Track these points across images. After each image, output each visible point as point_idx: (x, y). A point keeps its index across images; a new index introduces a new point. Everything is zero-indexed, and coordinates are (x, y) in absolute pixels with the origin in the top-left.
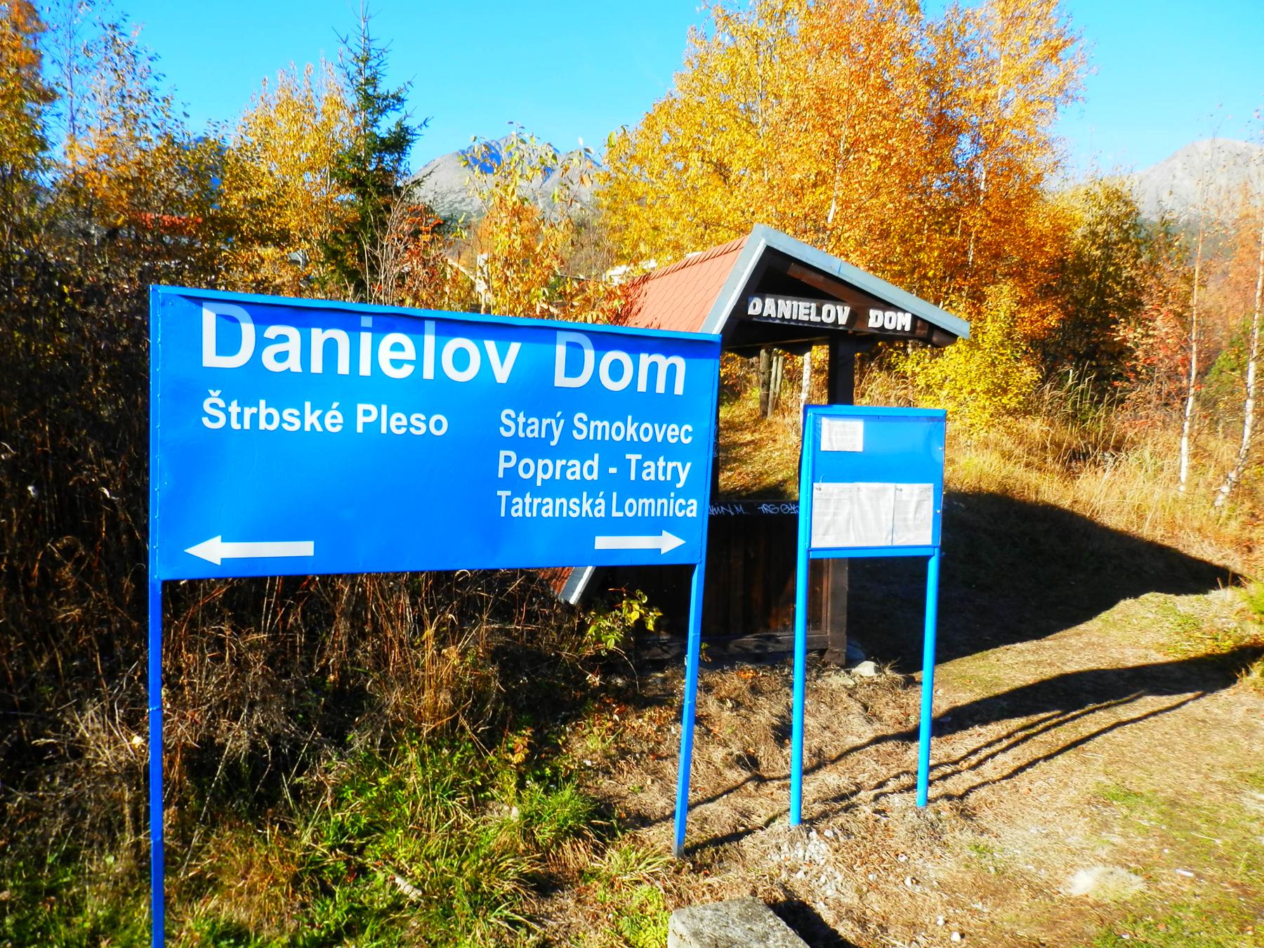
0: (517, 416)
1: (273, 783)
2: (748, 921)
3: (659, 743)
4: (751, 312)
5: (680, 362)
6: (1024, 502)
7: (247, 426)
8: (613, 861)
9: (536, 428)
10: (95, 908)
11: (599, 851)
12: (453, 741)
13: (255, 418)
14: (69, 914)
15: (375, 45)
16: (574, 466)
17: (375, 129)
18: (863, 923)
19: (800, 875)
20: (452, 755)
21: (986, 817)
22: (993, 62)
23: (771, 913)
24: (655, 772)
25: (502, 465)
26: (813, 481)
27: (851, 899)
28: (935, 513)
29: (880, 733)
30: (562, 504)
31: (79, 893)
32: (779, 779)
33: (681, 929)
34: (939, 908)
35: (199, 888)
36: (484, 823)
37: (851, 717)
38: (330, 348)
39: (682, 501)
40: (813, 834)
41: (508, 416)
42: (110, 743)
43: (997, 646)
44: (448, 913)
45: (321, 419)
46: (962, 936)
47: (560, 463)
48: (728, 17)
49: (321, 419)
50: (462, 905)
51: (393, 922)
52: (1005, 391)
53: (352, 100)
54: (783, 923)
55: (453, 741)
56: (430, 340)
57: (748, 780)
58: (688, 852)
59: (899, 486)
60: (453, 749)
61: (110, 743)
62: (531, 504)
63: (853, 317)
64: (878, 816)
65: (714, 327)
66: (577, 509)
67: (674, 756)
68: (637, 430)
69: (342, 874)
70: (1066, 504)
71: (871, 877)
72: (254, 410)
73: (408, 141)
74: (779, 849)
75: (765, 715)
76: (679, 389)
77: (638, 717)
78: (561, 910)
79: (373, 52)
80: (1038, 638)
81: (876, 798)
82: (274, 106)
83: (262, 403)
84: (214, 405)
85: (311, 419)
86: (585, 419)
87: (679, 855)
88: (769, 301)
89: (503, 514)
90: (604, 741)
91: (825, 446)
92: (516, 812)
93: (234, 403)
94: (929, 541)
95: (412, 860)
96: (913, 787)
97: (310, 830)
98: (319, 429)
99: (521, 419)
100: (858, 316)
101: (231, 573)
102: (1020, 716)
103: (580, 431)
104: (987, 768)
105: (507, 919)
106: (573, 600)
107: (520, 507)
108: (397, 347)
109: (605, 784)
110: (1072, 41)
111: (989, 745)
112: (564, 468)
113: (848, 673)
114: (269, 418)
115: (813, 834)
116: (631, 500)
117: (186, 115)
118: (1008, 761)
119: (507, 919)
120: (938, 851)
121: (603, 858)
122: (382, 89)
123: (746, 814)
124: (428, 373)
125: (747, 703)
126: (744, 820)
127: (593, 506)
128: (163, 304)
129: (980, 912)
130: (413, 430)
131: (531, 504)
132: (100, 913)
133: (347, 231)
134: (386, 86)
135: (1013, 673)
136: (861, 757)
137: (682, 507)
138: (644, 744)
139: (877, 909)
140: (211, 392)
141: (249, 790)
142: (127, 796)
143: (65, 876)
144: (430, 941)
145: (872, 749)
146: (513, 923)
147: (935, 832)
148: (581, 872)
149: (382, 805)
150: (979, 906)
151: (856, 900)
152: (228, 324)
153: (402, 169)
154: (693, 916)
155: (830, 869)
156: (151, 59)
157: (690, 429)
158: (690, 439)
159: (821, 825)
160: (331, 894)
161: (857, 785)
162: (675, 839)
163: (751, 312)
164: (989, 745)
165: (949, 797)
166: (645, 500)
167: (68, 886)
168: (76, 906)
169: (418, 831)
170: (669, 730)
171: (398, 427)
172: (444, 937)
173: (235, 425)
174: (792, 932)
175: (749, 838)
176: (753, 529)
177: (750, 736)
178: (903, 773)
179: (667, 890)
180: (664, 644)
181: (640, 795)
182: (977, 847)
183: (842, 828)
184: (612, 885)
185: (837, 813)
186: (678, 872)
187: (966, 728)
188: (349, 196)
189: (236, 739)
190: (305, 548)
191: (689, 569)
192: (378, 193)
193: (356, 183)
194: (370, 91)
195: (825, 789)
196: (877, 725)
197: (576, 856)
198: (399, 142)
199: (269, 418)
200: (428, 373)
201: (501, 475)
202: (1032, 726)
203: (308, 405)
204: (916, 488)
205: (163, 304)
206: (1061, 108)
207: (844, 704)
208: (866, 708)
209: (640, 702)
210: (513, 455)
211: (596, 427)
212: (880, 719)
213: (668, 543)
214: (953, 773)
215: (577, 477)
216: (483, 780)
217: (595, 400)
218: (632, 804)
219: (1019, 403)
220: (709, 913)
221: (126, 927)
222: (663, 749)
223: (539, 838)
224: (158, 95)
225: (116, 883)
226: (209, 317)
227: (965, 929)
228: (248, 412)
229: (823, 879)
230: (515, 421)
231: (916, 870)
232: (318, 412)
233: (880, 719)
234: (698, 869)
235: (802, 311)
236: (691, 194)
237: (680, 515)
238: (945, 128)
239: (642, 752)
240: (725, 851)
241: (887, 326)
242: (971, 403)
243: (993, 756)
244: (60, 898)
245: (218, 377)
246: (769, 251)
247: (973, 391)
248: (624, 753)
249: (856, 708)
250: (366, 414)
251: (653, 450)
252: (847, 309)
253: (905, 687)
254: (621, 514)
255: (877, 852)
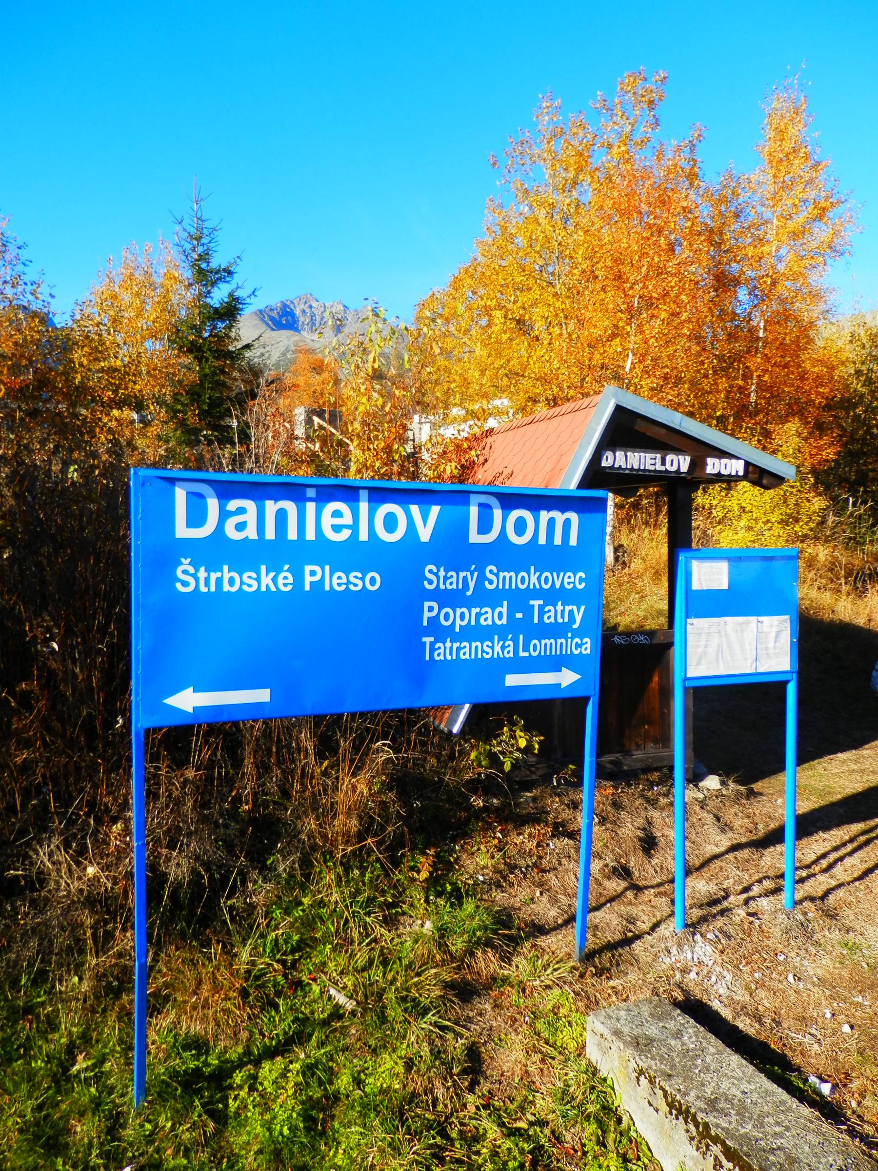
0: (438, 570)
1: (212, 905)
2: (660, 1019)
3: (540, 858)
4: (604, 464)
5: (573, 517)
6: (822, 620)
7: (213, 589)
8: (521, 966)
9: (454, 580)
10: (70, 1024)
11: (506, 959)
12: (361, 862)
13: (219, 581)
14: (46, 1032)
15: (207, 224)
16: (486, 613)
17: (208, 300)
18: (759, 1019)
19: (693, 975)
20: (363, 875)
21: (848, 916)
22: (767, 222)
23: (679, 1011)
24: (541, 885)
25: (426, 615)
26: (687, 617)
27: (742, 996)
28: (792, 642)
29: (735, 842)
30: (476, 647)
31: (53, 1011)
32: (652, 887)
33: (600, 1028)
34: (824, 1002)
35: (154, 1006)
36: (399, 936)
37: (706, 827)
38: (281, 516)
39: (577, 640)
40: (698, 937)
41: (431, 571)
42: (68, 874)
43: (821, 757)
44: (383, 1019)
45: (274, 580)
46: (852, 1027)
47: (474, 611)
48: (526, 191)
49: (274, 580)
50: (395, 1013)
51: (335, 1030)
52: (797, 520)
53: (188, 274)
54: (692, 1021)
55: (361, 862)
56: (364, 506)
57: (626, 889)
58: (588, 957)
59: (760, 618)
60: (363, 870)
61: (68, 874)
62: (451, 648)
63: (693, 465)
64: (751, 919)
65: (570, 482)
66: (490, 650)
67: (555, 869)
68: (539, 579)
69: (283, 987)
70: (861, 621)
71: (756, 975)
72: (219, 574)
73: (238, 309)
74: (669, 952)
75: (630, 828)
76: (573, 541)
77: (519, 834)
78: (480, 1014)
79: (205, 231)
80: (856, 747)
81: (746, 902)
82: (117, 283)
83: (226, 568)
84: (185, 572)
85: (266, 580)
86: (495, 571)
87: (581, 960)
88: (620, 454)
89: (427, 658)
90: (493, 857)
91: (695, 586)
92: (428, 925)
93: (202, 569)
94: (787, 667)
95: (342, 973)
96: (777, 890)
97: (248, 948)
98: (273, 589)
99: (442, 573)
100: (697, 464)
101: (203, 719)
102: (858, 821)
103: (491, 582)
104: (838, 869)
105: (435, 1024)
106: (456, 729)
107: (442, 651)
108: (337, 514)
109: (499, 896)
110: (840, 202)
111: (836, 849)
112: (478, 615)
113: (696, 786)
114: (231, 582)
115: (698, 937)
116: (535, 641)
117: (52, 296)
118: (856, 863)
119: (435, 1024)
120: (812, 949)
121: (510, 965)
122: (214, 264)
123: (631, 920)
124: (363, 536)
125: (612, 818)
126: (631, 927)
127: (503, 648)
128: (143, 484)
129: (861, 1005)
130: (351, 587)
131: (451, 648)
132: (75, 1030)
133: (187, 393)
134: (217, 261)
135: (842, 782)
136: (723, 864)
137: (578, 646)
138: (528, 859)
139: (767, 1005)
140: (183, 560)
141: (192, 915)
142: (88, 922)
143: (39, 996)
144: (370, 1047)
145: (730, 856)
146: (443, 1028)
147: (805, 930)
148: (494, 979)
149: (309, 923)
150: (860, 999)
151: (747, 997)
152: (196, 501)
153: (233, 335)
154: (610, 1017)
155: (718, 969)
156: (19, 248)
157: (584, 576)
158: (583, 584)
159: (704, 928)
160: (276, 1007)
161: (724, 890)
162: (577, 942)
163: (604, 464)
164: (836, 849)
165: (812, 899)
166: (547, 641)
167: (43, 1004)
168: (52, 1025)
169: (344, 944)
170: (548, 845)
171: (339, 585)
172: (382, 1042)
173: (203, 589)
174: (702, 1029)
175: (638, 942)
176: (634, 661)
177: (620, 848)
178: (765, 878)
179: (577, 994)
180: (533, 766)
181: (532, 906)
182: (846, 945)
183: (721, 931)
184: (524, 990)
185: (714, 916)
186: (582, 976)
187: (811, 834)
188: (187, 360)
189: (178, 868)
190: (263, 695)
191: (584, 701)
192: (214, 357)
193: (194, 349)
194: (204, 266)
195: (698, 895)
196: (730, 834)
197: (487, 963)
198: (230, 311)
199: (231, 582)
200: (363, 536)
201: (425, 623)
202: (871, 830)
203: (263, 568)
204: (768, 621)
205: (143, 484)
206: (829, 261)
207: (696, 814)
208: (718, 820)
209: (521, 821)
210: (435, 605)
211: (504, 577)
212: (731, 829)
213: (567, 678)
214: (809, 877)
215: (489, 622)
216: (393, 896)
217: (503, 554)
218: (525, 914)
219: (811, 530)
220: (622, 1013)
221: (97, 1041)
222: (545, 863)
223: (453, 949)
224: (26, 278)
225: (85, 1001)
226: (180, 495)
227: (853, 1021)
228: (214, 576)
229: (714, 979)
230: (436, 575)
231: (795, 967)
232: (272, 574)
233: (731, 829)
234: (600, 972)
235: (649, 461)
236: (496, 349)
237: (576, 652)
238: (724, 283)
239: (528, 866)
240: (620, 955)
241: (723, 472)
242: (766, 533)
243: (841, 859)
244: (38, 1016)
245: (190, 547)
246: (619, 409)
247: (768, 521)
248: (512, 868)
249: (709, 819)
250: (312, 573)
251: (552, 596)
252: (688, 459)
253: (748, 798)
254: (527, 654)
255: (758, 952)
